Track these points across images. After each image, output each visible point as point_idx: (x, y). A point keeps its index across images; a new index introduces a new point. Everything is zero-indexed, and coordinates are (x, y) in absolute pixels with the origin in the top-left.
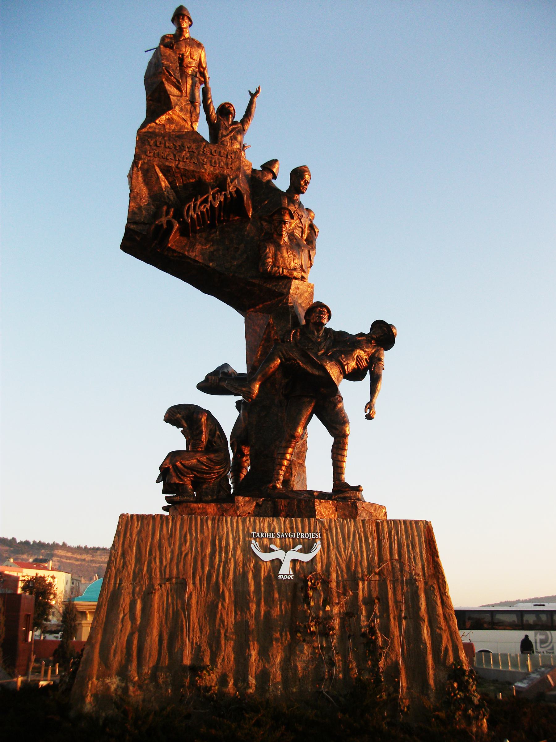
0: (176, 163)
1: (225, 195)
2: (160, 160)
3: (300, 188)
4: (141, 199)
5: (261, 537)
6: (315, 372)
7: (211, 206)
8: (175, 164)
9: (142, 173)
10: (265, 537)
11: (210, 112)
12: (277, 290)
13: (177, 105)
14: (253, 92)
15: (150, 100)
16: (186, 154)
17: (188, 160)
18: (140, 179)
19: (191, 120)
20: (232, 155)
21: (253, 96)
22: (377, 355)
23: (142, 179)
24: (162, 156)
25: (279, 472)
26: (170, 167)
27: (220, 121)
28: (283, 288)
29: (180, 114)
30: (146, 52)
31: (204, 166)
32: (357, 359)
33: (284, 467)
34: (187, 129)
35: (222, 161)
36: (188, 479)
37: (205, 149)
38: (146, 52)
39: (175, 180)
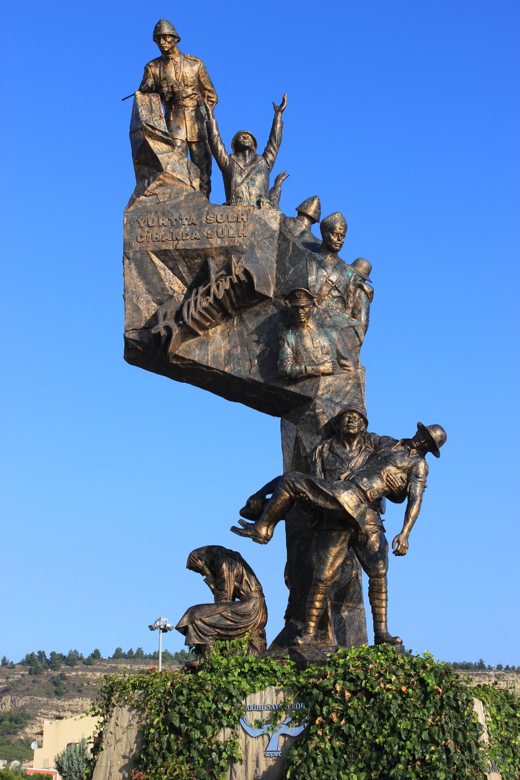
0: (175, 244)
1: (231, 280)
2: (155, 244)
3: (331, 245)
4: (138, 298)
5: (251, 710)
6: (330, 506)
7: (215, 297)
8: (173, 245)
9: (135, 265)
10: (255, 709)
11: (218, 154)
12: (302, 394)
13: (168, 164)
14: (278, 104)
15: (138, 163)
16: (185, 228)
17: (188, 237)
18: (134, 273)
19: (189, 178)
20: (243, 217)
21: (278, 109)
22: (414, 470)
23: (137, 272)
24: (157, 238)
25: (309, 624)
26: (167, 250)
27: (233, 164)
28: (309, 390)
29: (174, 175)
30: (123, 100)
31: (209, 241)
32: (387, 480)
33: (315, 617)
34: (186, 191)
35: (231, 228)
36: (211, 637)
37: (208, 217)
38: (123, 100)
39: (177, 265)
